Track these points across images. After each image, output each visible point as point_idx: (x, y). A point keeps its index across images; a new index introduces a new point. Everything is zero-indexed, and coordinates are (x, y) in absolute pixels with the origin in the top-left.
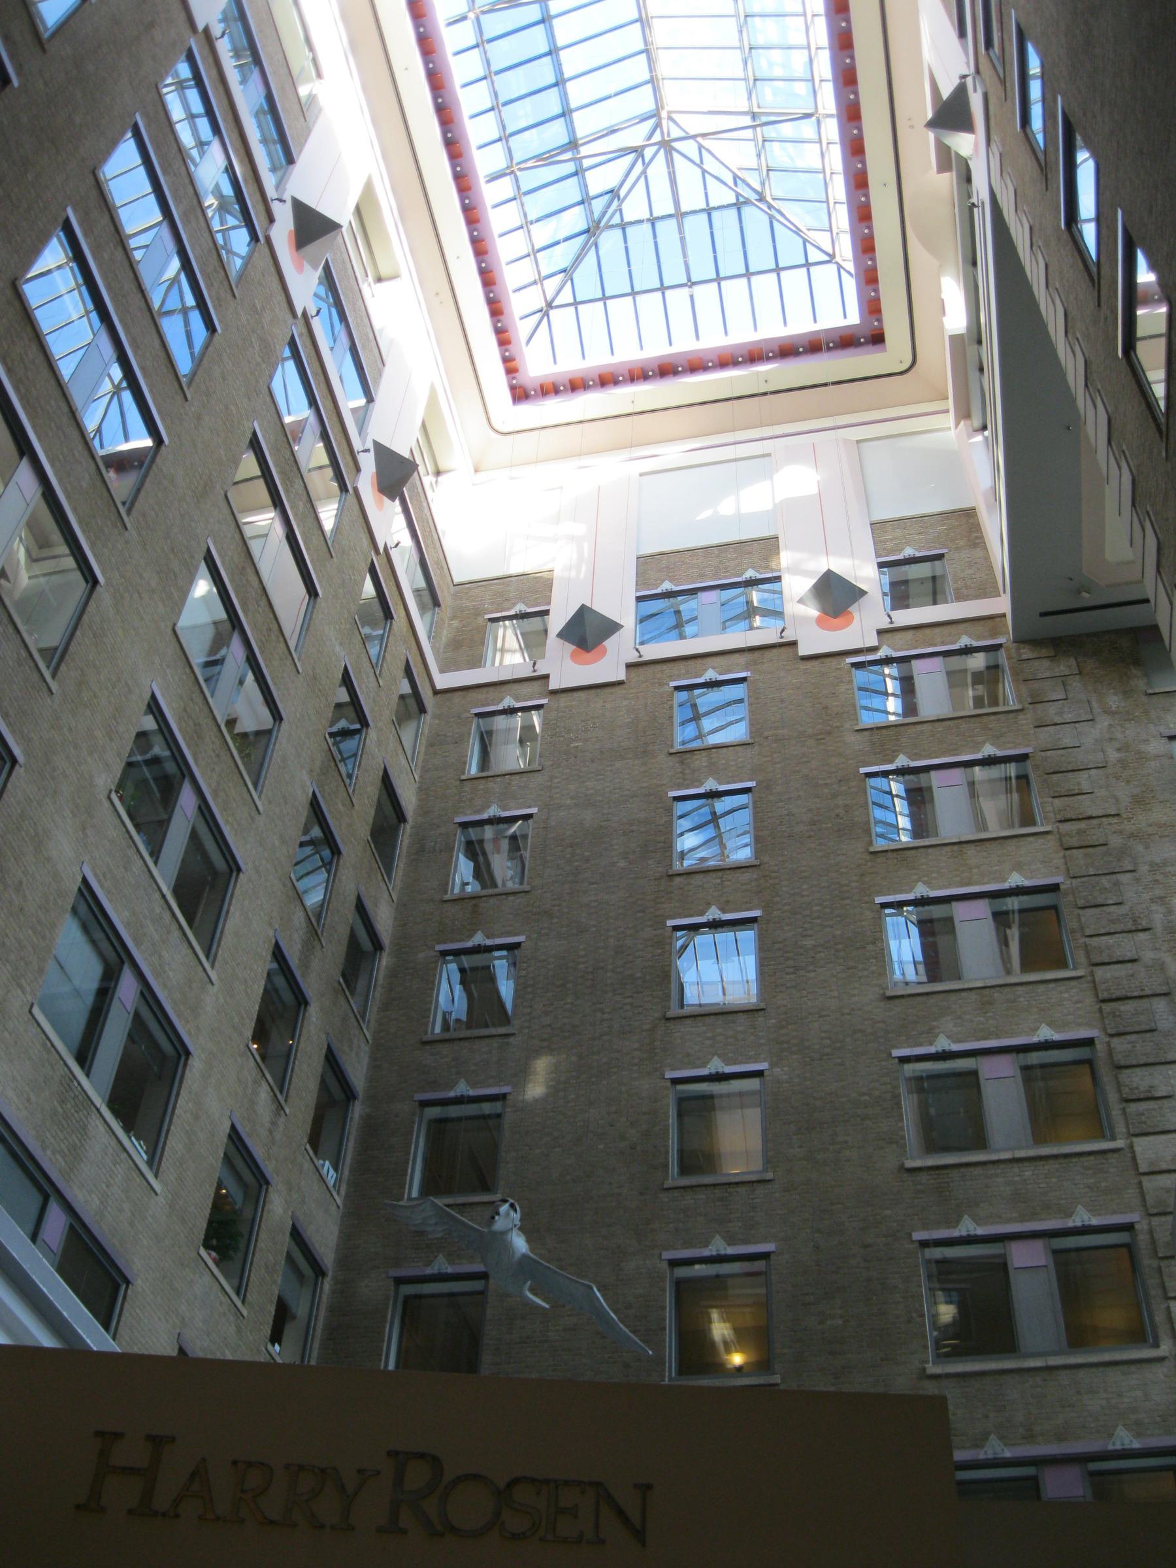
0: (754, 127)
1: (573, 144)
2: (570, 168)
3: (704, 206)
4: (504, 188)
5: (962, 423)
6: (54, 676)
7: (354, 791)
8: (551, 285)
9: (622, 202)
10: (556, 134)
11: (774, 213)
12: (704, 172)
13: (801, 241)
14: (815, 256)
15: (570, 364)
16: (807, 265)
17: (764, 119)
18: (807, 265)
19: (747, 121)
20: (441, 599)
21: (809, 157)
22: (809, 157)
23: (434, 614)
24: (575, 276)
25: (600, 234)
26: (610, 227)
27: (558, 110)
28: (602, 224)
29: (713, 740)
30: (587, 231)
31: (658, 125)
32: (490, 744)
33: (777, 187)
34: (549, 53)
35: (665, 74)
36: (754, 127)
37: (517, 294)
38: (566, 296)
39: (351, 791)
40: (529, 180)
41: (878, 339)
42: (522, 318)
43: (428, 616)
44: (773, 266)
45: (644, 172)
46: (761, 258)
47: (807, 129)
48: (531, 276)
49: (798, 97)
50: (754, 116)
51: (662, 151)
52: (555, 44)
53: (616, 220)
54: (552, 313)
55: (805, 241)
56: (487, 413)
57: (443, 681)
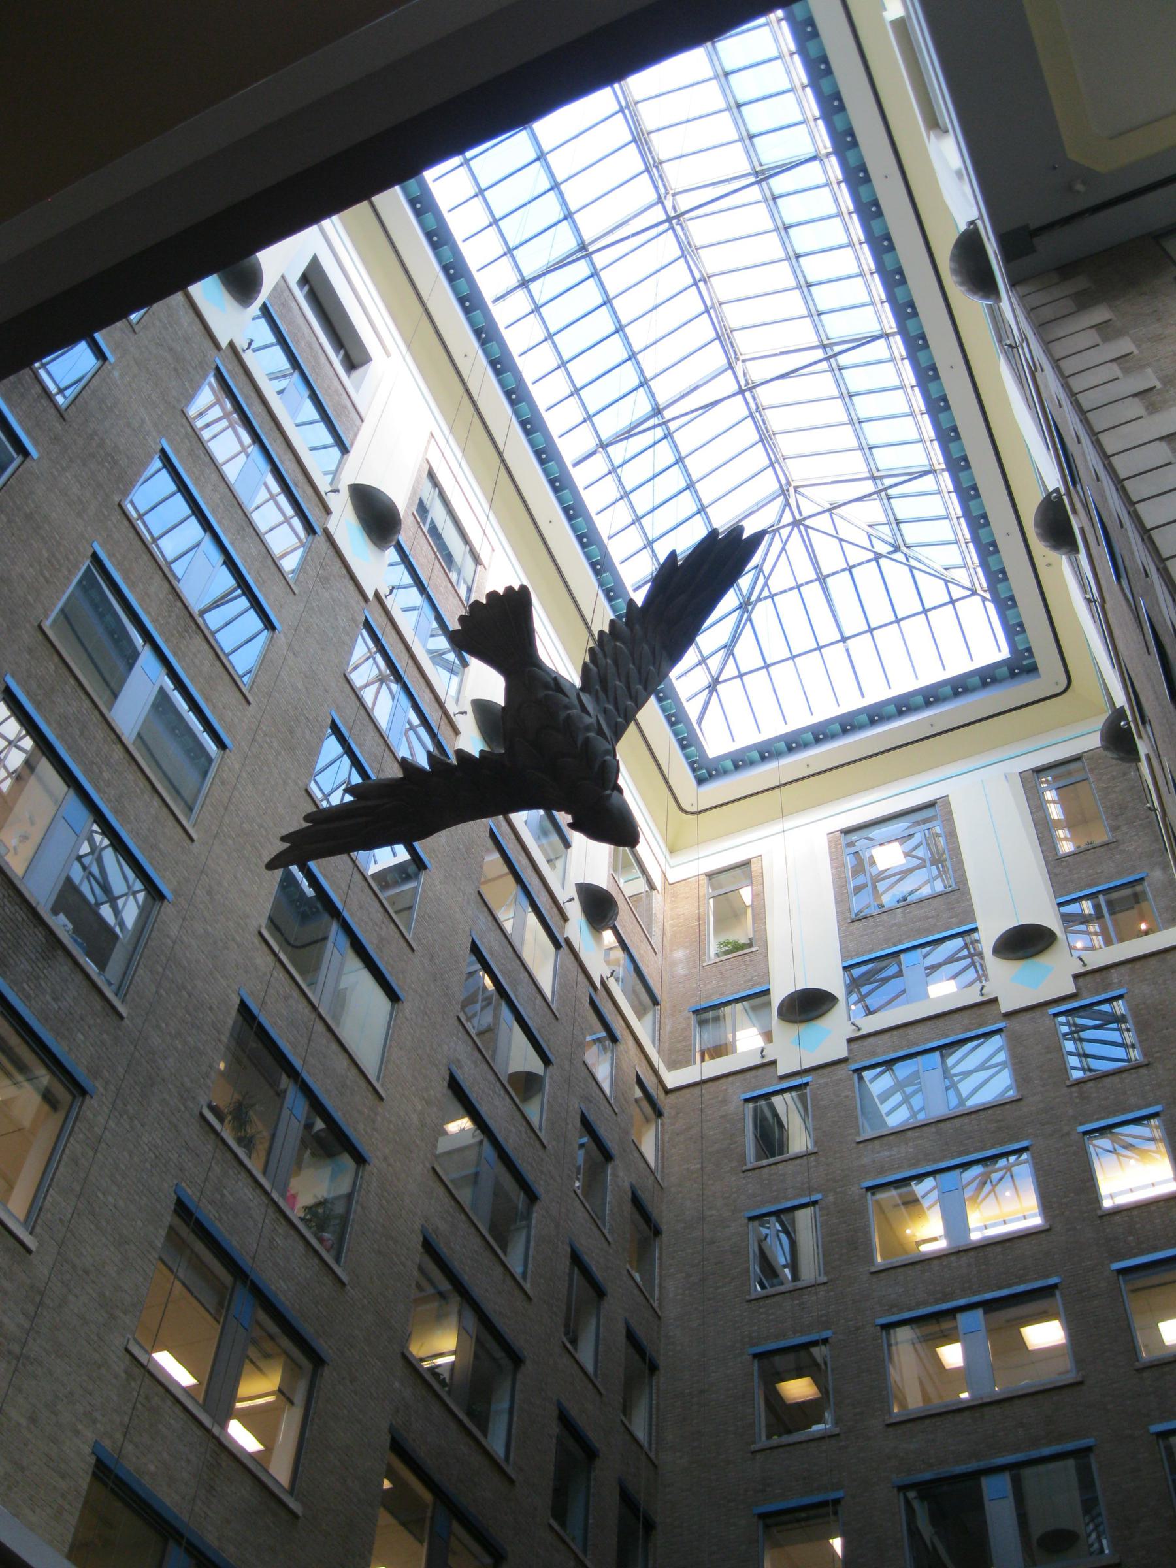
0: (827, 359)
1: (583, 250)
2: (659, 432)
3: (845, 566)
4: (598, 464)
5: (932, 133)
6: (337, 1260)
7: (660, 1304)
8: (714, 663)
9: (767, 579)
10: (640, 405)
11: (913, 563)
12: (841, 540)
13: (942, 582)
14: (957, 592)
15: (747, 737)
16: (952, 602)
17: (837, 349)
18: (952, 602)
19: (819, 354)
20: (658, 997)
21: (934, 506)
22: (886, 375)
23: (655, 1011)
24: (735, 651)
25: (753, 609)
26: (759, 599)
27: (635, 382)
28: (753, 599)
29: (972, 1103)
30: (740, 607)
31: (787, 504)
32: (794, 1231)
33: (911, 533)
34: (688, 488)
35: (650, 128)
36: (827, 359)
37: (501, 303)
38: (730, 670)
39: (656, 1305)
40: (618, 452)
41: (1033, 669)
42: (597, 514)
43: (649, 1018)
44: (921, 609)
45: (783, 549)
46: (907, 603)
47: (928, 482)
48: (591, 443)
49: (915, 457)
50: (757, 174)
51: (796, 529)
52: (644, 377)
53: (766, 593)
54: (719, 687)
55: (946, 582)
56: (406, 271)
57: (673, 1079)
